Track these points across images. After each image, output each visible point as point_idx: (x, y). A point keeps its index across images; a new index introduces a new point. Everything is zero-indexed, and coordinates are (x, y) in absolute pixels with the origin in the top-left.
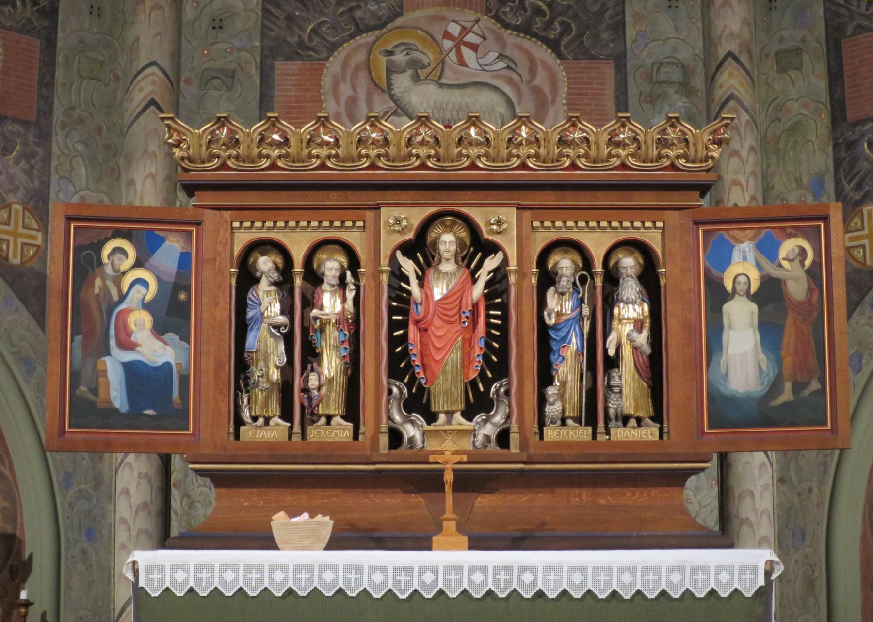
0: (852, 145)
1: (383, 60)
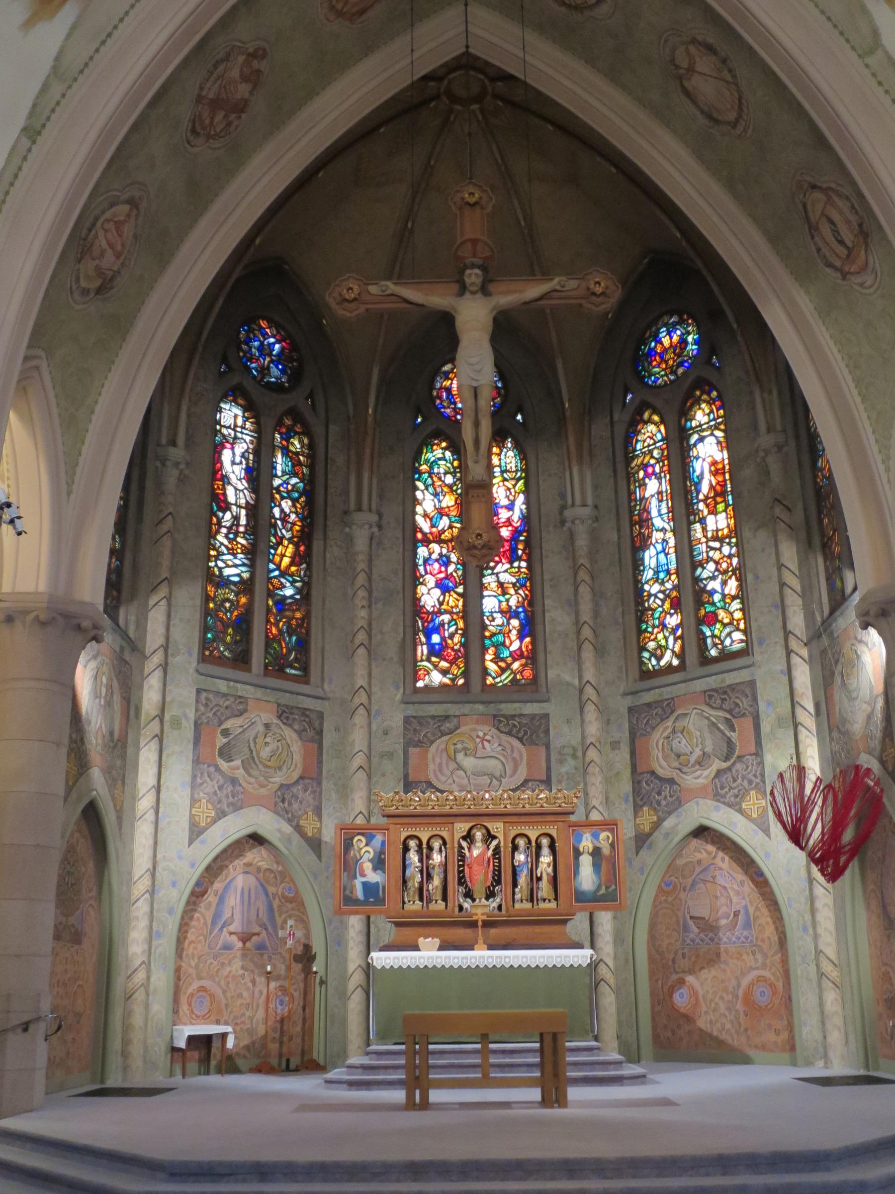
0: (639, 782)
1: (452, 747)
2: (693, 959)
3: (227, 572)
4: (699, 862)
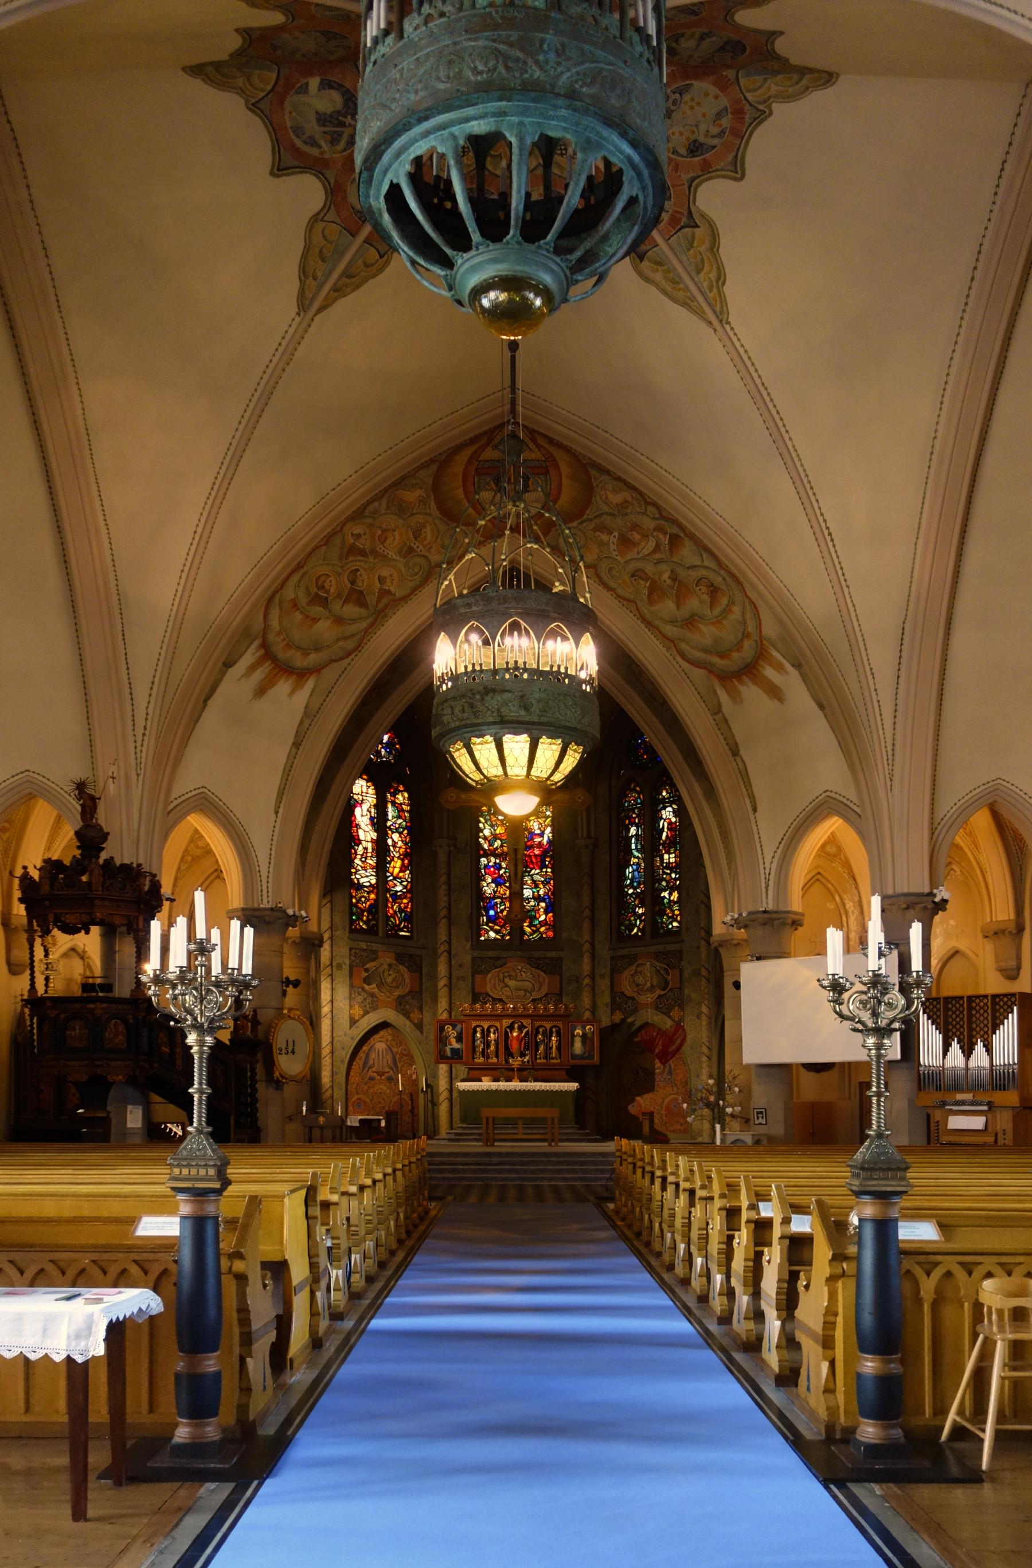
3: (362, 881)
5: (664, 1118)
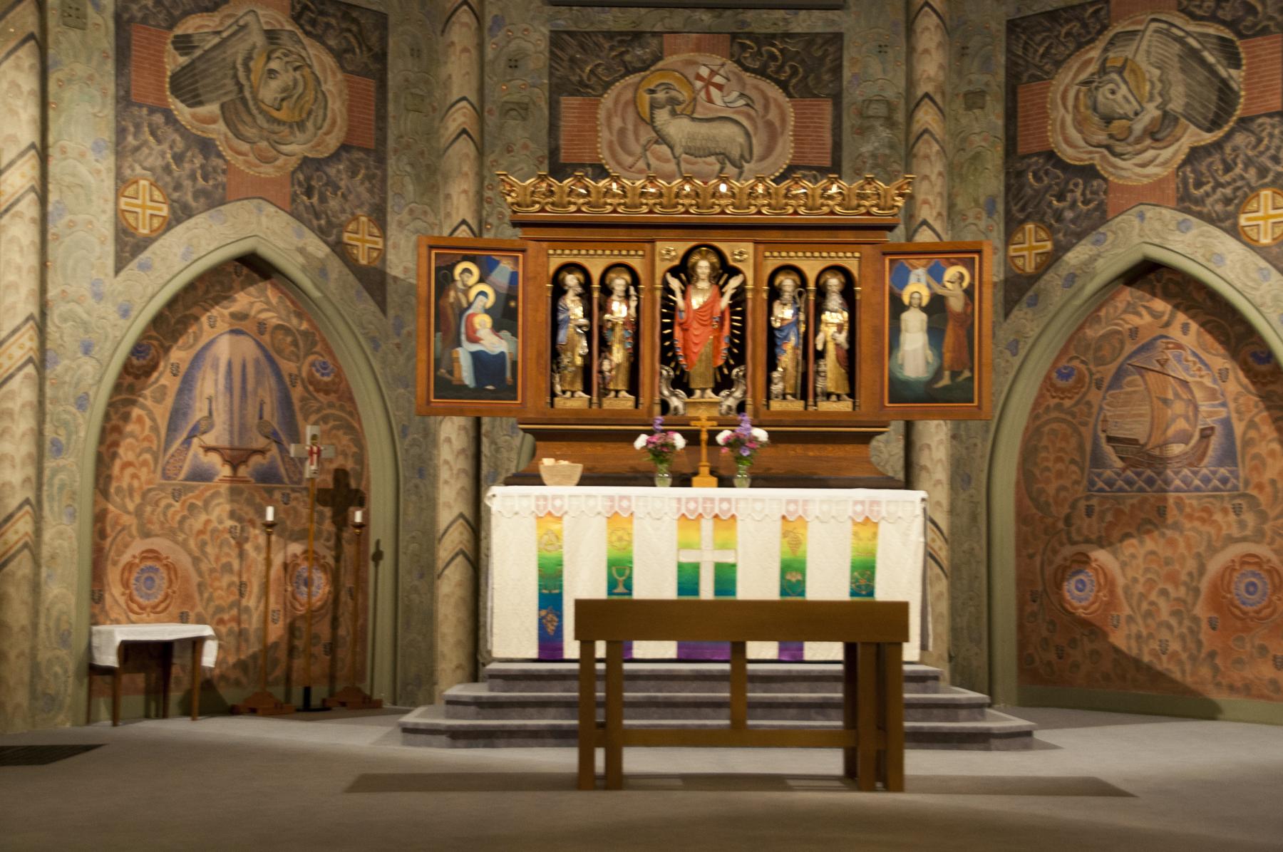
0: (1020, 174)
1: (647, 97)
2: (1109, 517)
4: (1134, 332)
5: (1205, 634)
